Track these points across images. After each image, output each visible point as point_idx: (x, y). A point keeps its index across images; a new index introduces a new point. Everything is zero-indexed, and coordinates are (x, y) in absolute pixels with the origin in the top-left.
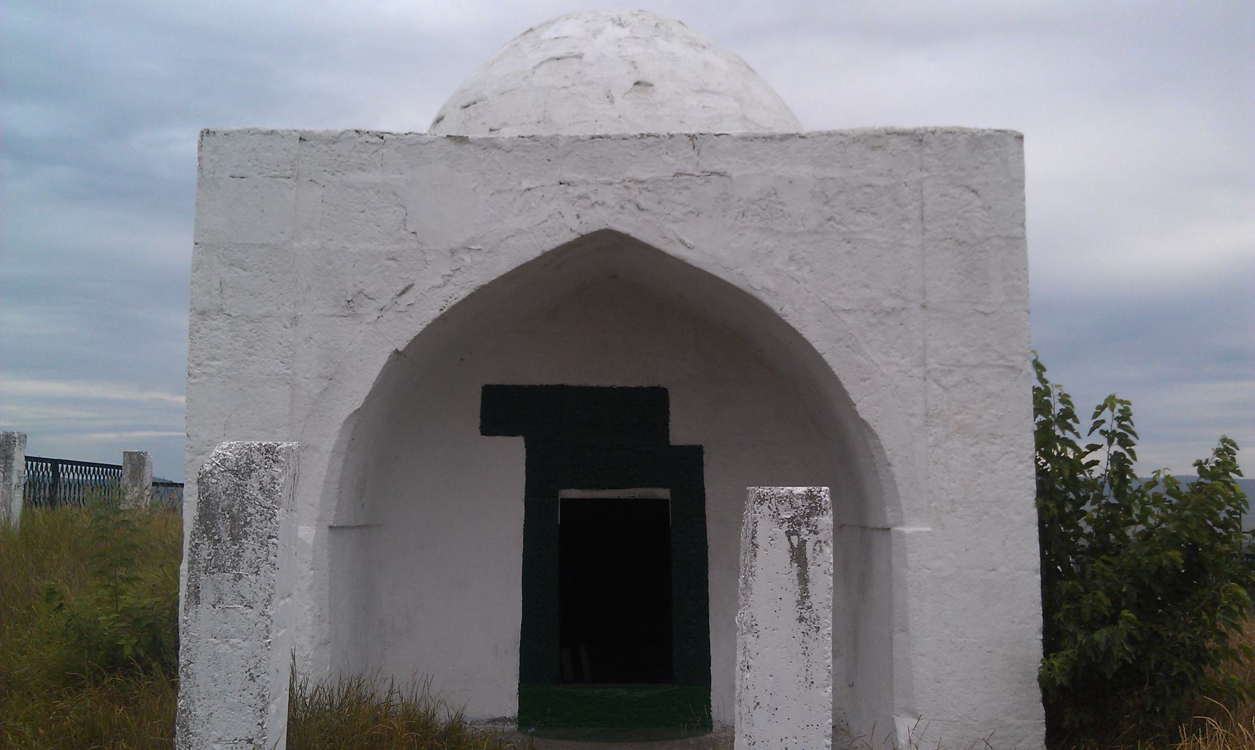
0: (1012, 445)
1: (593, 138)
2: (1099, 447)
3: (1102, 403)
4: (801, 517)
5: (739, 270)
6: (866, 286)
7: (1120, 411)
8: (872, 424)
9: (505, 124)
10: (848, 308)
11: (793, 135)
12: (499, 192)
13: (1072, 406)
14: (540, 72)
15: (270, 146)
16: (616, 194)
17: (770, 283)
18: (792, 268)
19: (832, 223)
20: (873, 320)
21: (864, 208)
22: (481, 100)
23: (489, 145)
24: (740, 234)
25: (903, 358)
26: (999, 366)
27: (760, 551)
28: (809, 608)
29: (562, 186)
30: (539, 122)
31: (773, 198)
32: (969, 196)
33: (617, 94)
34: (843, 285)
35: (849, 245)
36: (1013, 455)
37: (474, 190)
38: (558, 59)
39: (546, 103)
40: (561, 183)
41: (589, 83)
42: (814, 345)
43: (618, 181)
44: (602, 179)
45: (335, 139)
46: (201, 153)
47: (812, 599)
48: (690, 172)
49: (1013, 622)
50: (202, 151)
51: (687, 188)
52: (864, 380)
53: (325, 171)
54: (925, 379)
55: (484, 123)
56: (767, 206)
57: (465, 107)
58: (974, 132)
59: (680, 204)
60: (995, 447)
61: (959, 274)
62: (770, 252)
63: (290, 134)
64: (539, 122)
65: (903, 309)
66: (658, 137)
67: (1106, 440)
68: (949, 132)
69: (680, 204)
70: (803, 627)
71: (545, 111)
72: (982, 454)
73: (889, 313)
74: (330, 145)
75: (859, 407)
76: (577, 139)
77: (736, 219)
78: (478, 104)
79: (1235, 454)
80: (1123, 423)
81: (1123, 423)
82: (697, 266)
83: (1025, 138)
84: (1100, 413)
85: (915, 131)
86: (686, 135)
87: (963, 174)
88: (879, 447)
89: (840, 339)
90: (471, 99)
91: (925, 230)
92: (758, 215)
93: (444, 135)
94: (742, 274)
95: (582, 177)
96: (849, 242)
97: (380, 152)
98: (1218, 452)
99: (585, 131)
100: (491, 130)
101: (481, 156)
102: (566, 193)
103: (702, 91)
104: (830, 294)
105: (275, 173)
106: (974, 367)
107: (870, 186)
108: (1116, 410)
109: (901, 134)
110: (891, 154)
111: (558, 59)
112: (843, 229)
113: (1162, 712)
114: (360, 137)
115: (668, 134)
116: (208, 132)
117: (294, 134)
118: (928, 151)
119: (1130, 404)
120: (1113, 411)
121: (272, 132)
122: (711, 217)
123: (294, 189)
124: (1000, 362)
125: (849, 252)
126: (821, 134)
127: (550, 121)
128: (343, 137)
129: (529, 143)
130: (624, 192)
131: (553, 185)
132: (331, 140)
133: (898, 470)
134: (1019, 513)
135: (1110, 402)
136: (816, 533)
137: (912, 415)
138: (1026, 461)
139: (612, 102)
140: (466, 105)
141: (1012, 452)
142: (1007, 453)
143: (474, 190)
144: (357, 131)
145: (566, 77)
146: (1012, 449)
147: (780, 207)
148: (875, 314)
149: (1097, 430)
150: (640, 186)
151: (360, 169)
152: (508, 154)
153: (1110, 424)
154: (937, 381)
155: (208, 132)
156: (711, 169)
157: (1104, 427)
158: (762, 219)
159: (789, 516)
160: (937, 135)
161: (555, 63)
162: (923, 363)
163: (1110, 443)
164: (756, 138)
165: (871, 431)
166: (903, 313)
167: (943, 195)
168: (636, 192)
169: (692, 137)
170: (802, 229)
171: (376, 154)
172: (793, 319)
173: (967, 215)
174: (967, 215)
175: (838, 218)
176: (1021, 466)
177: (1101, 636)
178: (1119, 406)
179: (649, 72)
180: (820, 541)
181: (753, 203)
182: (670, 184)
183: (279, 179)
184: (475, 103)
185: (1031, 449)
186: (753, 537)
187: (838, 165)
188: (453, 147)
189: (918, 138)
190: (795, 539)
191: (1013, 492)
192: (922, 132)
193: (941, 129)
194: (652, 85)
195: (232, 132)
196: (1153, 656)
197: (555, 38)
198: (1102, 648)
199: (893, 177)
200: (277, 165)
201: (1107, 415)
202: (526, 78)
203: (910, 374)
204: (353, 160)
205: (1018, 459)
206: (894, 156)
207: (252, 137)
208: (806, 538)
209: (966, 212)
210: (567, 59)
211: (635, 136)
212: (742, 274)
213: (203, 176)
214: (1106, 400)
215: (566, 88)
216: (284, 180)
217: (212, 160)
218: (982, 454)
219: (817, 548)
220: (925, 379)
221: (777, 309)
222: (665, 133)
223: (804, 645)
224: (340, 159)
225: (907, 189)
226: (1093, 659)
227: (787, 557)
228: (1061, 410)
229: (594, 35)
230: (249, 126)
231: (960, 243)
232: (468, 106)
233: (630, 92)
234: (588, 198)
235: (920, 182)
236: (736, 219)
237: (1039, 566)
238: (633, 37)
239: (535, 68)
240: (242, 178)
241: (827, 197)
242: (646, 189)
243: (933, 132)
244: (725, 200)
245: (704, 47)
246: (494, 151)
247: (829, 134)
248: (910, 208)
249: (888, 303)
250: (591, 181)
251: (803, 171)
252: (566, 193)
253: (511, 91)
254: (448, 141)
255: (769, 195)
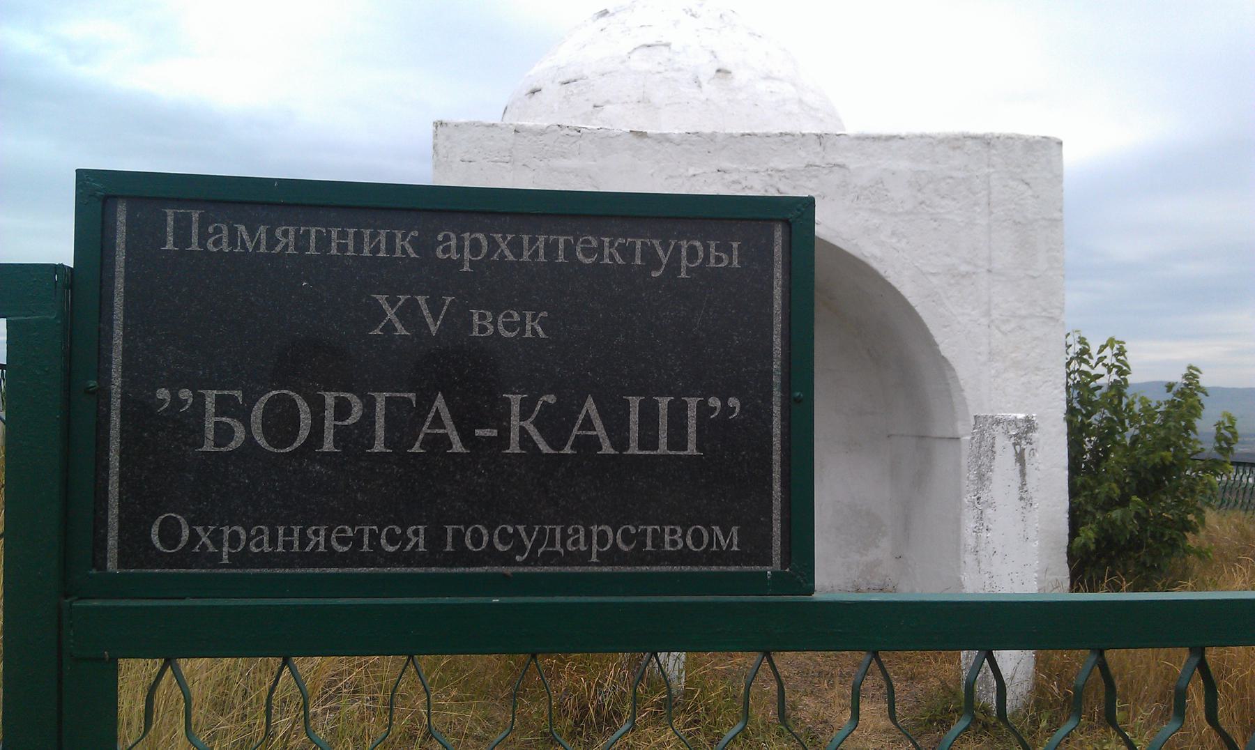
0: (1050, 376)
1: (743, 135)
2: (1102, 376)
3: (1105, 343)
4: (1022, 433)
5: (855, 242)
6: (948, 255)
7: (1118, 349)
8: (950, 360)
9: (608, 102)
10: (933, 272)
11: (894, 137)
12: (671, 177)
13: (1088, 345)
14: (635, 56)
15: (492, 137)
16: (762, 180)
17: (877, 251)
18: (894, 240)
19: (923, 206)
20: (952, 282)
21: (947, 195)
22: (581, 79)
23: (664, 139)
24: (855, 214)
25: (974, 309)
26: (1042, 317)
27: (997, 456)
28: (1026, 491)
29: (719, 173)
30: (639, 102)
31: (880, 186)
32: (1023, 187)
33: (702, 79)
34: (931, 254)
35: (935, 223)
36: (1051, 383)
37: (652, 175)
38: (649, 46)
39: (644, 86)
40: (719, 171)
41: (679, 70)
42: (909, 300)
43: (763, 170)
44: (751, 168)
45: (542, 132)
46: (436, 141)
47: (1027, 485)
48: (817, 164)
49: (1048, 506)
50: (437, 139)
51: (816, 177)
52: (945, 327)
53: (535, 157)
54: (989, 326)
55: (587, 100)
56: (876, 191)
57: (565, 84)
58: (1028, 137)
59: (811, 189)
60: (1038, 377)
61: (1016, 247)
62: (878, 228)
63: (507, 127)
64: (639, 102)
65: (974, 273)
66: (793, 135)
67: (1106, 370)
68: (1009, 138)
69: (811, 189)
70: (1023, 503)
71: (644, 92)
72: (1029, 383)
73: (963, 276)
74: (538, 137)
75: (942, 347)
76: (731, 136)
77: (852, 201)
78: (579, 82)
79: (1198, 378)
80: (1119, 357)
81: (1119, 357)
82: (822, 238)
83: (1064, 144)
84: (1103, 351)
85: (985, 135)
86: (814, 134)
87: (1019, 170)
88: (955, 378)
89: (929, 296)
90: (571, 76)
91: (991, 213)
92: (869, 198)
93: (628, 130)
94: (856, 245)
95: (735, 166)
96: (935, 221)
97: (578, 143)
98: (1185, 376)
99: (737, 130)
100: (595, 106)
101: (657, 148)
102: (723, 179)
103: (768, 77)
104: (921, 261)
105: (496, 158)
106: (1024, 317)
107: (951, 178)
108: (1115, 349)
109: (974, 138)
110: (966, 153)
111: (649, 46)
112: (931, 210)
113: (1159, 565)
114: (562, 130)
115: (801, 133)
116: (442, 123)
117: (511, 126)
118: (994, 151)
119: (1124, 343)
120: (1112, 349)
121: (493, 124)
122: (833, 200)
123: (512, 172)
124: (1043, 314)
125: (935, 229)
126: (916, 136)
127: (649, 102)
128: (549, 129)
129: (694, 138)
130: (767, 178)
131: (712, 172)
132: (539, 133)
133: (968, 394)
134: (1054, 426)
135: (1111, 342)
136: (1031, 444)
137: (979, 353)
138: (1060, 388)
139: (700, 86)
140: (566, 81)
141: (1050, 381)
142: (1046, 381)
143: (652, 175)
144: (559, 126)
145: (660, 63)
146: (1050, 378)
147: (885, 193)
148: (954, 276)
149: (1101, 363)
150: (780, 174)
151: (562, 156)
152: (678, 147)
153: (1110, 360)
154: (998, 328)
155: (442, 123)
156: (834, 162)
157: (1105, 361)
158: (871, 202)
159: (1014, 433)
160: (1001, 139)
161: (646, 51)
162: (988, 313)
163: (1110, 371)
164: (867, 138)
165: (949, 365)
166: (974, 276)
167: (1004, 186)
168: (777, 179)
169: (819, 136)
170: (901, 210)
171: (574, 145)
172: (893, 278)
173: (1022, 202)
174: (1022, 202)
175: (928, 203)
176: (1056, 392)
177: (1116, 514)
178: (1117, 346)
179: (726, 61)
180: (1033, 449)
181: (865, 189)
182: (803, 173)
183: (499, 164)
184: (575, 81)
185: (1063, 379)
186: (993, 447)
187: (928, 161)
188: (635, 141)
189: (987, 142)
190: (1018, 447)
191: (1049, 410)
192: (990, 136)
193: (1004, 136)
194: (730, 73)
195: (461, 124)
196: (1148, 528)
197: (641, 26)
198: (1118, 523)
199: (968, 171)
200: (498, 152)
201: (1108, 352)
202: (623, 62)
203: (978, 322)
204: (556, 149)
205: (1054, 386)
206: (969, 155)
207: (477, 128)
208: (1025, 447)
209: (1022, 199)
210: (657, 47)
211: (776, 134)
212: (856, 245)
213: (438, 160)
214: (1108, 342)
215: (659, 73)
216: (504, 165)
217: (445, 147)
218: (1029, 383)
219: (1032, 453)
220: (989, 326)
221: (882, 272)
222: (798, 132)
223: (1023, 515)
224: (546, 148)
225: (978, 181)
226: (1110, 531)
227: (1013, 459)
228: (1080, 349)
229: (674, 25)
230: (473, 120)
231: (1016, 223)
232: (568, 83)
233: (714, 78)
234: (740, 183)
235: (988, 176)
236: (852, 201)
237: (1067, 465)
238: (707, 28)
239: (629, 53)
240: (470, 162)
241: (920, 185)
242: (785, 177)
243: (998, 138)
244: (844, 186)
245: (760, 36)
246: (667, 144)
247: (922, 137)
248: (979, 195)
249: (964, 268)
250: (742, 169)
251: (903, 165)
252: (723, 179)
253: (610, 72)
254: (631, 135)
255: (877, 183)
